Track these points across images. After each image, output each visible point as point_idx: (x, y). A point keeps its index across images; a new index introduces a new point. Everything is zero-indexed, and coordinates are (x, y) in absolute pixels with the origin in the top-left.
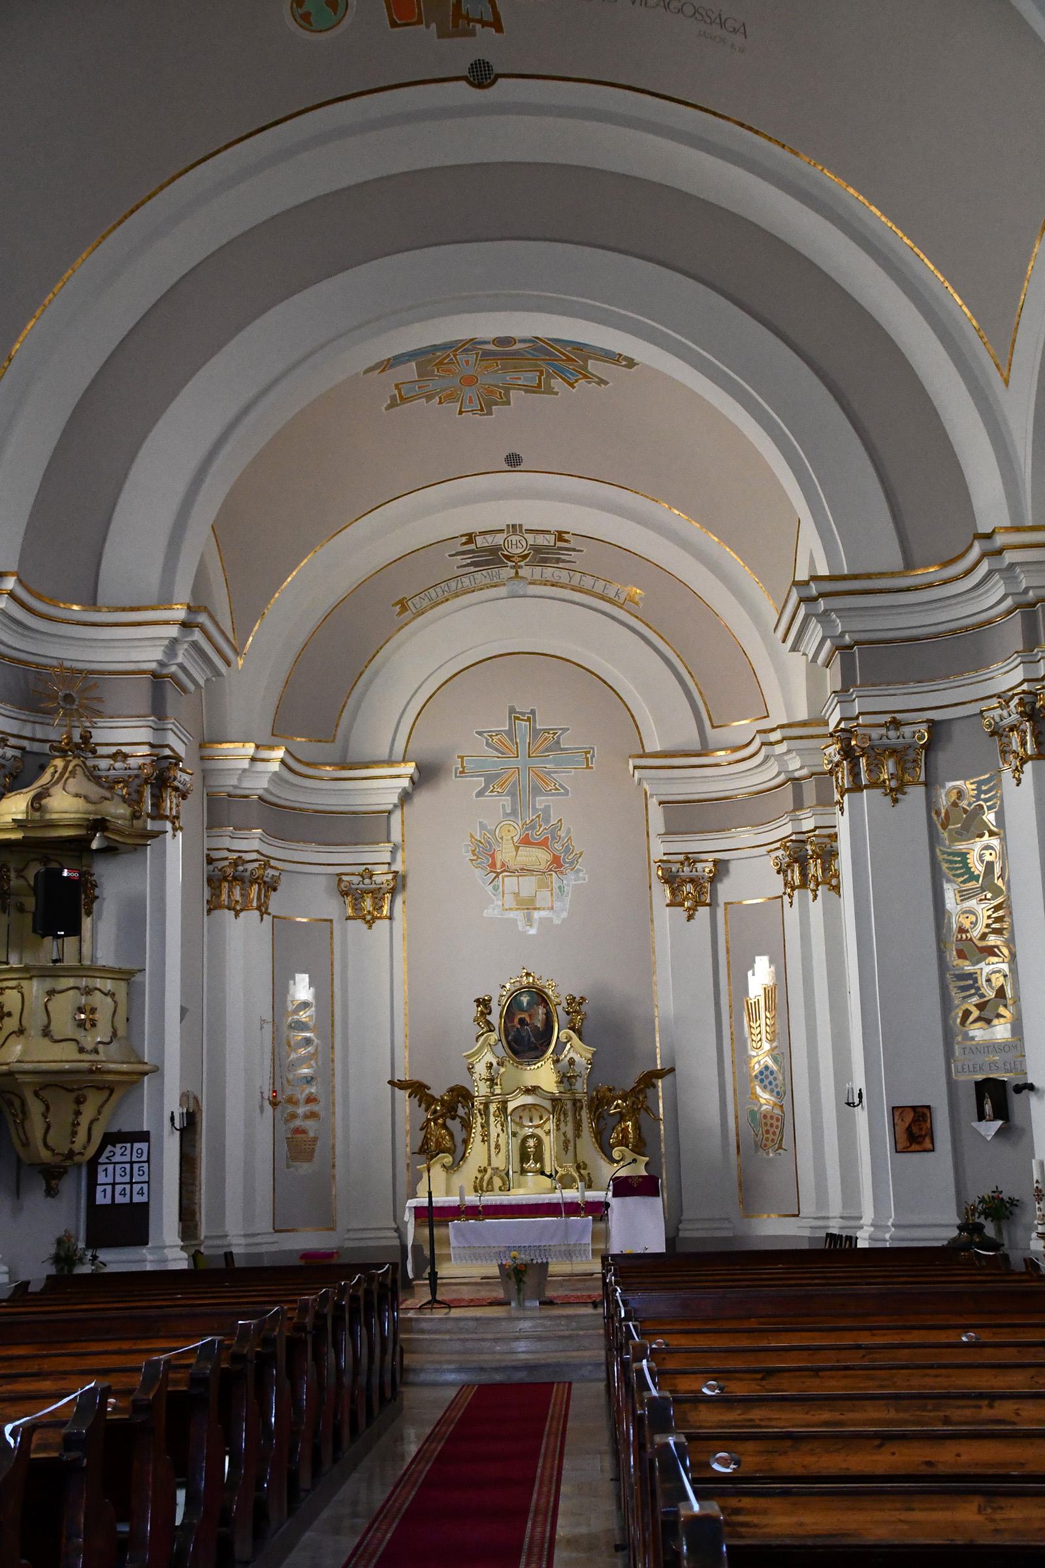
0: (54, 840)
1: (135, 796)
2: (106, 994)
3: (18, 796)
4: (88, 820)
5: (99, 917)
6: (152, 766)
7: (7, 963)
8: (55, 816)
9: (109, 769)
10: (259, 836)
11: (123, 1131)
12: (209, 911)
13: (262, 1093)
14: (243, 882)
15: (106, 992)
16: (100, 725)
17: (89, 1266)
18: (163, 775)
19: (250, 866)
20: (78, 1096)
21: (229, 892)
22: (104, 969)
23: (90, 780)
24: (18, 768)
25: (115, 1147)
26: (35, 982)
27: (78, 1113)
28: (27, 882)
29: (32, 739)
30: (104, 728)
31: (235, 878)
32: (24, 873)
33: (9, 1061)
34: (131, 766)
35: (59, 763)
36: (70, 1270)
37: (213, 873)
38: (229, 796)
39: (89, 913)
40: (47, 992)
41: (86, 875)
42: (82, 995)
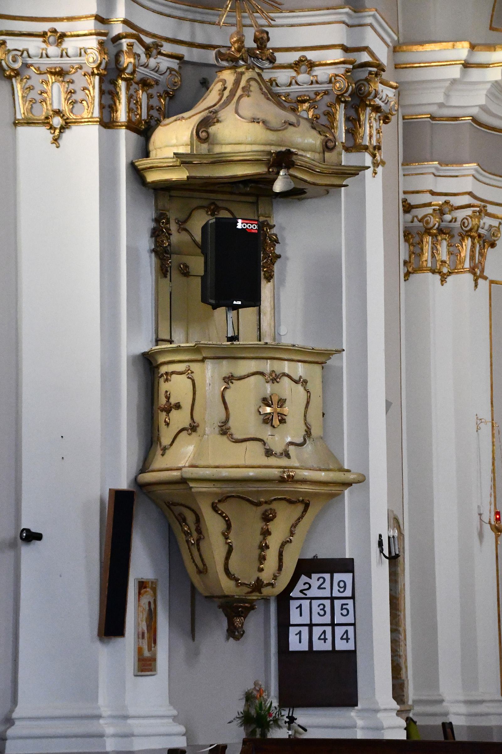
0: (226, 180)
1: (323, 120)
2: (296, 382)
3: (178, 122)
4: (269, 153)
5: (282, 282)
6: (347, 78)
7: (171, 342)
8: (227, 149)
9: (290, 84)
10: (473, 172)
11: (319, 557)
12: (407, 275)
13: (480, 515)
14: (452, 237)
15: (297, 378)
16: (279, 21)
17: (285, 730)
18: (360, 90)
19: (461, 214)
20: (266, 511)
21: (432, 248)
22: (292, 349)
23: (268, 99)
24: (175, 84)
25: (310, 578)
26: (209, 365)
27: (266, 533)
28: (191, 236)
29: (191, 45)
30: (282, 26)
31: (441, 231)
32: (188, 226)
33: (180, 465)
34: (320, 79)
35: (228, 76)
36: (264, 734)
37: (411, 225)
38: (433, 118)
39: (269, 278)
40: (224, 379)
41: (264, 226)
42: (267, 382)
